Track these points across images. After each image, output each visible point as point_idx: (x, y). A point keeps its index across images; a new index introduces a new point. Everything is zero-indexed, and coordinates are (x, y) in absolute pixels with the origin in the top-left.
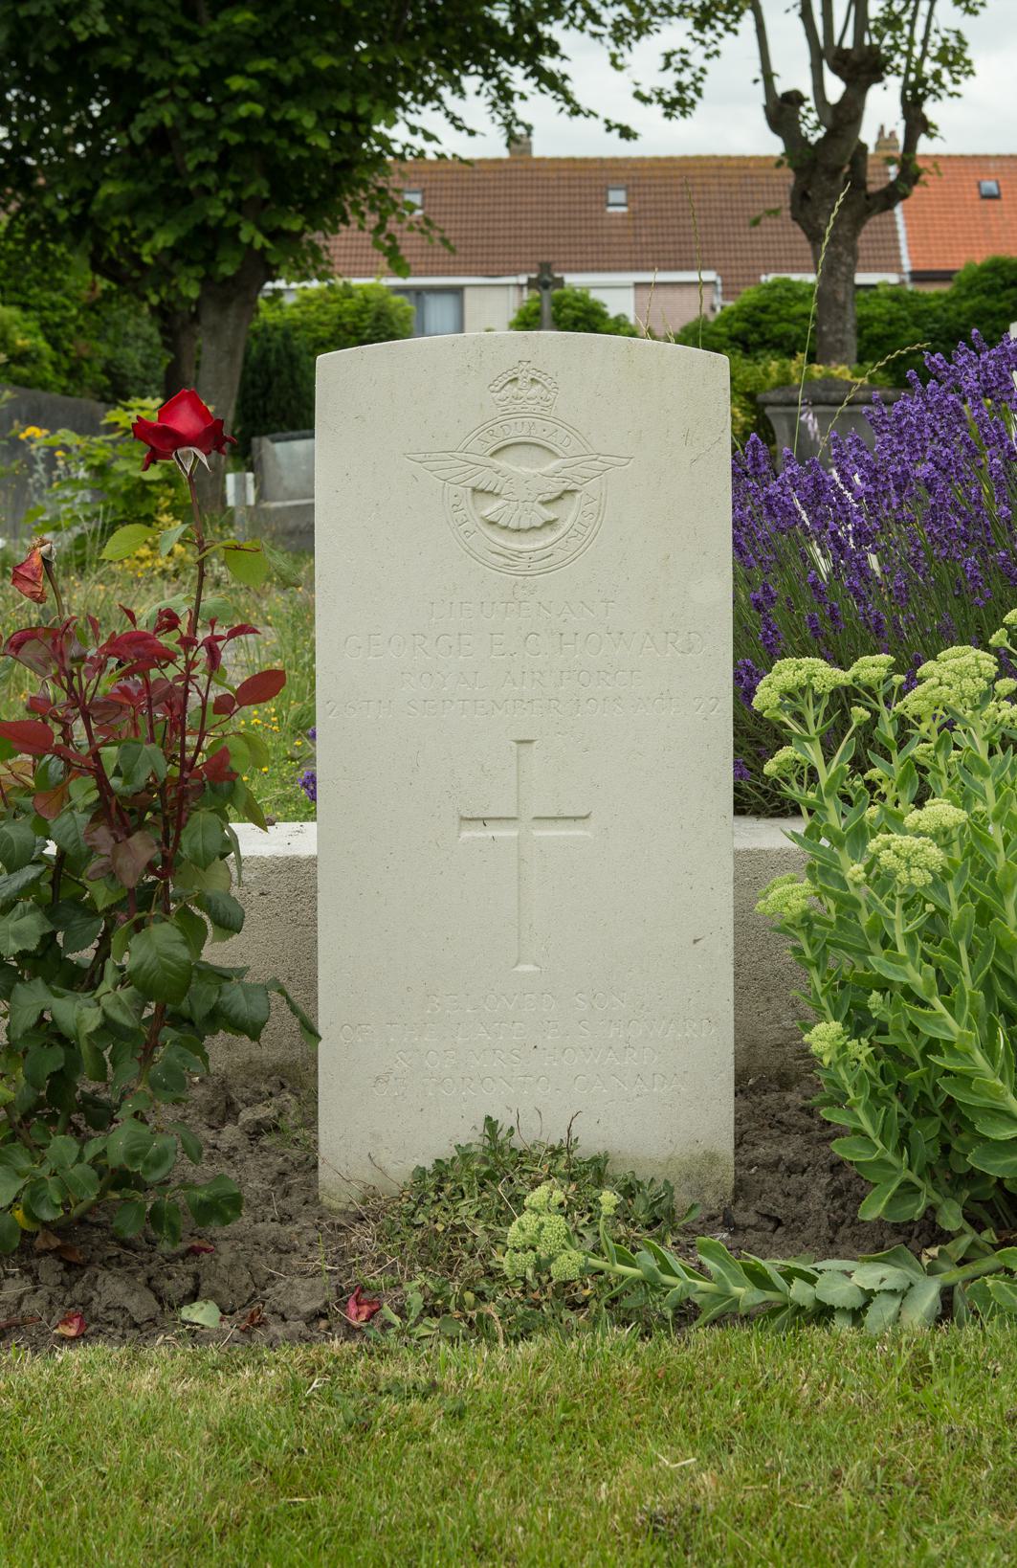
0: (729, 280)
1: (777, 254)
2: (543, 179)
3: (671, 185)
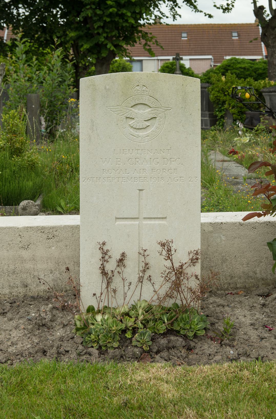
0: (215, 58)
1: (229, 51)
2: (164, 30)
3: (199, 32)
